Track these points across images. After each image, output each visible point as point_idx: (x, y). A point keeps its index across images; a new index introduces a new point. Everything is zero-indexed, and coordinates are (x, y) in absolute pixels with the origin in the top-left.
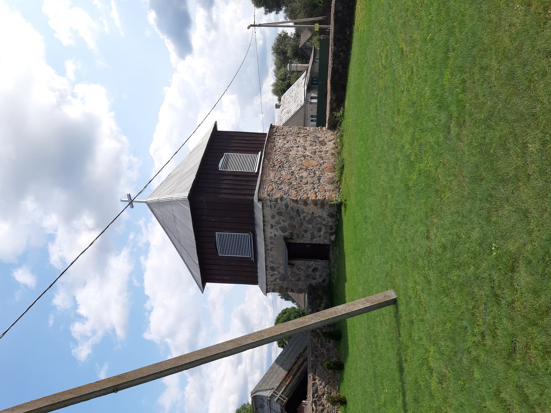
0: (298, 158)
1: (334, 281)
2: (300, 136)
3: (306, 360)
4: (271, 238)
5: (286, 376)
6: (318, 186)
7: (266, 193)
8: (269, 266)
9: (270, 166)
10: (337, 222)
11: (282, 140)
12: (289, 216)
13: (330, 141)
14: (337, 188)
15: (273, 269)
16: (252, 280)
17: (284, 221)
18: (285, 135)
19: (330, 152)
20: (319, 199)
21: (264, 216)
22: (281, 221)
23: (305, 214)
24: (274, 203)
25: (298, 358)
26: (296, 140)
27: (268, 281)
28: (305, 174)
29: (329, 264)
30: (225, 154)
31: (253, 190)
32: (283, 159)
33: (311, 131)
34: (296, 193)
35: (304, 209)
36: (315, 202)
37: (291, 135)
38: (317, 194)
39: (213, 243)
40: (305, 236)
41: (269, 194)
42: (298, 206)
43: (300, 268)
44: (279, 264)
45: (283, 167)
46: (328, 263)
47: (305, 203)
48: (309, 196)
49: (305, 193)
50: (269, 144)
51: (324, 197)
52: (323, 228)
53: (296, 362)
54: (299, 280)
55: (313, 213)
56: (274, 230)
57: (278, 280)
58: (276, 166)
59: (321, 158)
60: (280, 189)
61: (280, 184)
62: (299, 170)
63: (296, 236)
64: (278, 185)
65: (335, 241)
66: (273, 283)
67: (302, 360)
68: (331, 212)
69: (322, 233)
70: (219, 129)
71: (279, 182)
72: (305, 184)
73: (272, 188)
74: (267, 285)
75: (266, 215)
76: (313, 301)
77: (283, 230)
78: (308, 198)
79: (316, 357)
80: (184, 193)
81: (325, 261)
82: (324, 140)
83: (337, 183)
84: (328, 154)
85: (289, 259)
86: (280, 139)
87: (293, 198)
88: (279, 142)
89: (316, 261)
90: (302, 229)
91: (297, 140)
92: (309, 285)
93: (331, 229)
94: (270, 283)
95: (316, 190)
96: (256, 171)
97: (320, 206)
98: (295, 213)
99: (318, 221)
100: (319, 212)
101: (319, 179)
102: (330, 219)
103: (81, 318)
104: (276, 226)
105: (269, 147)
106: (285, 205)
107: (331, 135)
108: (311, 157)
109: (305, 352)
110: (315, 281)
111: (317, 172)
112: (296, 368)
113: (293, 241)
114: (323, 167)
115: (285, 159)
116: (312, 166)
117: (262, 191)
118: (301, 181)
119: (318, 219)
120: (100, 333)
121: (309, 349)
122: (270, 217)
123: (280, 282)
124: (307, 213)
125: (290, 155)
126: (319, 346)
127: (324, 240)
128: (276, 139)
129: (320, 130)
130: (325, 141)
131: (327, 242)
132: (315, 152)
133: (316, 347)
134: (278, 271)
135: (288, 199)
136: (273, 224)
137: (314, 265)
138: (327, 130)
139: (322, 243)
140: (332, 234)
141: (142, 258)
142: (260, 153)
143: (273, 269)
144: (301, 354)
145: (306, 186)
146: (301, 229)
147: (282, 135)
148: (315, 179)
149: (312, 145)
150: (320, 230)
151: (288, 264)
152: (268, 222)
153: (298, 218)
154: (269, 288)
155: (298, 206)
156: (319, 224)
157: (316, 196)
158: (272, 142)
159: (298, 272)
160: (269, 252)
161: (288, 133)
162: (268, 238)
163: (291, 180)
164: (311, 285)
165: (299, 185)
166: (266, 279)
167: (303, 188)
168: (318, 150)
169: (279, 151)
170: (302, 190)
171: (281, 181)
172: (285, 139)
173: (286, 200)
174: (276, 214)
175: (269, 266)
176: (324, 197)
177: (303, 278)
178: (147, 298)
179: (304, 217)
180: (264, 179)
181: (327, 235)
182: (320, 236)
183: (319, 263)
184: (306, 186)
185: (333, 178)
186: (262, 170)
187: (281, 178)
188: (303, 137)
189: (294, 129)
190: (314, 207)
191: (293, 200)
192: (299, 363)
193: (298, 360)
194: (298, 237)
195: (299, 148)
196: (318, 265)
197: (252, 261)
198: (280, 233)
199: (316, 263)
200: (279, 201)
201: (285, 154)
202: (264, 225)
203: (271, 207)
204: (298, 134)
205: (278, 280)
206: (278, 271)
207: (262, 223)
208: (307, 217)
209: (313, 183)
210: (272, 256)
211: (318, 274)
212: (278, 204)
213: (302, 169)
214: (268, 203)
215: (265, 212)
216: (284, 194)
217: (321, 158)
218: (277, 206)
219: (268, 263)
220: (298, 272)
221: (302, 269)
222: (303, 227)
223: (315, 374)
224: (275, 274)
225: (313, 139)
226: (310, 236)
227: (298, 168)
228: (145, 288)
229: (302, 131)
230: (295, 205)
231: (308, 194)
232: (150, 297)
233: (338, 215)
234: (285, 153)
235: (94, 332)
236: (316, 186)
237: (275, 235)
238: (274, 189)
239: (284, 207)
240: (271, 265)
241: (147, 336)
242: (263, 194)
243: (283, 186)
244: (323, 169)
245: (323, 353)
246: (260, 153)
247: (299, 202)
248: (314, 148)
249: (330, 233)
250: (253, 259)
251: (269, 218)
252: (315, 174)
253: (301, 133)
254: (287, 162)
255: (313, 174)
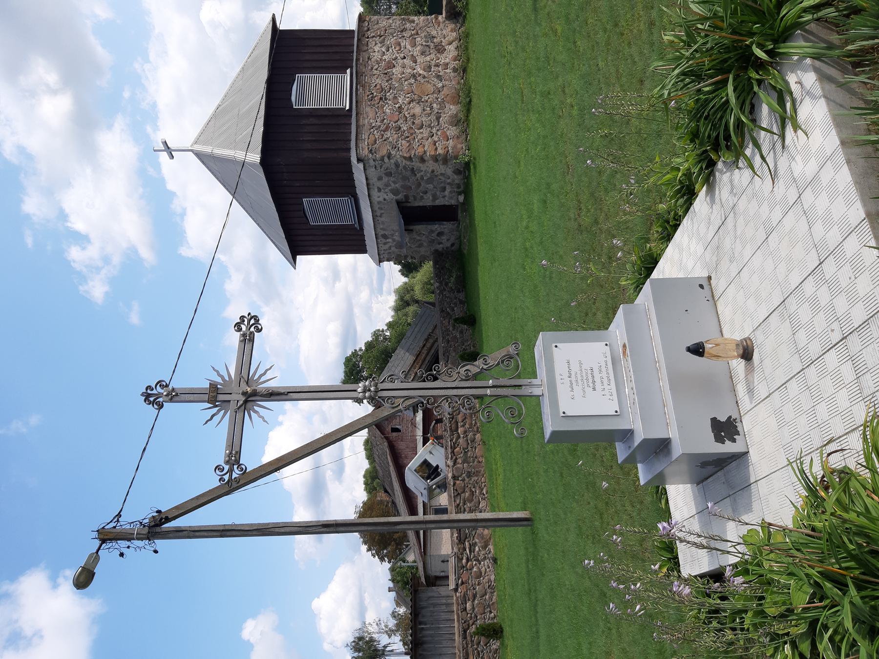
0: (405, 81)
1: (465, 252)
2: (405, 35)
3: (436, 341)
4: (379, 203)
5: (414, 362)
6: (438, 130)
7: (367, 147)
8: (380, 234)
9: (366, 98)
10: (466, 180)
11: (379, 45)
12: (401, 176)
13: (450, 43)
14: (463, 132)
15: (385, 237)
16: (359, 248)
17: (395, 182)
18: (382, 36)
19: (451, 66)
20: (439, 154)
21: (367, 179)
22: (391, 182)
23: (422, 173)
24: (380, 162)
25: (427, 340)
26: (400, 45)
27: (371, 184)
28: (417, 110)
29: (458, 227)
30: (297, 75)
31: (347, 141)
32: (385, 84)
33: (421, 25)
34: (408, 144)
35: (420, 167)
36: (435, 159)
37: (392, 34)
38: (437, 144)
39: (301, 211)
40: (425, 197)
41: (371, 150)
42: (412, 164)
43: (421, 233)
44: (393, 231)
45: (386, 99)
46: (456, 225)
47: (422, 160)
48: (426, 149)
49: (421, 144)
50: (361, 56)
51: (447, 149)
52: (448, 187)
53: (424, 345)
54: (420, 246)
55: (433, 171)
56: (383, 194)
57: (394, 248)
58: (376, 98)
59: (439, 77)
60: (385, 140)
61: (384, 131)
62: (410, 103)
63: (412, 198)
64: (382, 133)
65: (463, 204)
66: (387, 252)
67: (431, 341)
68: (457, 169)
69: (447, 193)
70: (282, 27)
71: (383, 127)
72: (419, 129)
73: (373, 139)
74: (379, 254)
75: (370, 177)
76: (440, 272)
77: (395, 192)
78: (425, 152)
79: (448, 342)
80: (251, 154)
81: (452, 222)
82: (441, 42)
83: (463, 122)
84: (448, 71)
85: (405, 224)
86: (376, 44)
87: (405, 155)
88: (376, 50)
89: (440, 225)
90: (420, 191)
91: (402, 44)
92: (434, 250)
93: (459, 187)
94: (382, 252)
95: (435, 138)
96: (347, 108)
97: (441, 162)
98: (408, 173)
99: (440, 179)
100: (441, 169)
101: (438, 118)
102: (455, 177)
103: (81, 239)
104: (384, 189)
105: (361, 61)
106: (395, 163)
107: (452, 31)
108: (424, 77)
109: (434, 332)
110: (441, 246)
111: (435, 105)
112: (425, 351)
113: (409, 205)
114: (441, 96)
115: (387, 84)
116: (426, 94)
117: (360, 145)
118: (414, 123)
119: (441, 177)
120: (116, 260)
121: (438, 332)
122: (376, 179)
123: (396, 250)
124: (425, 172)
125: (393, 74)
126: (451, 329)
127: (450, 201)
128: (370, 46)
129: (434, 22)
130: (443, 44)
131: (453, 202)
132: (430, 67)
133: (448, 330)
134: (393, 239)
135: (398, 156)
136: (381, 187)
137: (439, 229)
138: (445, 21)
139: (447, 203)
140: (460, 193)
141: (149, 129)
142: (348, 71)
143: (385, 237)
144: (430, 335)
145: (420, 133)
146: (419, 191)
147: (379, 36)
148: (433, 117)
149: (425, 52)
150: (444, 189)
151: (406, 230)
152: (374, 185)
153: (413, 178)
154: (382, 257)
155: (413, 164)
156: (442, 182)
157: (436, 149)
158: (364, 51)
159: (418, 238)
160: (379, 218)
161: (386, 30)
162: (376, 203)
163: (399, 123)
164: (436, 251)
165: (412, 131)
166: (378, 248)
167: (417, 136)
168: (433, 62)
169: (376, 69)
170: (417, 140)
171: (385, 126)
172: (382, 42)
173: (395, 158)
174: (384, 175)
175: (380, 234)
176: (447, 149)
177: (425, 244)
178: (173, 194)
179: (422, 176)
180: (361, 124)
181: (453, 194)
182: (444, 197)
183: (445, 226)
184: (420, 133)
185: (456, 115)
186: (357, 106)
187: (385, 119)
188: (410, 37)
189: (395, 21)
190: (435, 164)
191: (405, 158)
192: (428, 345)
193: (426, 342)
194: (415, 198)
195: (405, 60)
196: (444, 228)
197: (356, 229)
198: (391, 196)
199: (442, 226)
200: (386, 160)
201: (386, 74)
202: (368, 189)
203: (375, 167)
204: (402, 31)
205: (393, 249)
206: (393, 239)
207: (366, 188)
208: (425, 176)
209: (430, 126)
210: (383, 223)
211: (444, 238)
212: (385, 163)
213: (412, 101)
214: (372, 163)
215: (368, 174)
216: (392, 148)
217: (439, 77)
218: (384, 166)
219: (378, 230)
220: (418, 238)
221: (424, 234)
222: (421, 187)
223: (447, 362)
224: (389, 242)
225: (425, 42)
226: (431, 198)
227: (407, 99)
228: (166, 179)
229: (408, 25)
230: (408, 163)
231: (424, 146)
232: (177, 194)
233: (467, 172)
234: (386, 71)
235: (106, 260)
236: (434, 130)
237: (385, 199)
238: (378, 139)
239: (393, 166)
240: (383, 232)
241: (184, 252)
242: (363, 151)
243: (389, 134)
244: (443, 99)
245: (456, 337)
246: (348, 71)
247: (414, 160)
248: (428, 58)
249: (457, 192)
250: (357, 226)
251: (374, 180)
252: (432, 108)
253: (406, 29)
254: (390, 88)
255: (428, 109)
